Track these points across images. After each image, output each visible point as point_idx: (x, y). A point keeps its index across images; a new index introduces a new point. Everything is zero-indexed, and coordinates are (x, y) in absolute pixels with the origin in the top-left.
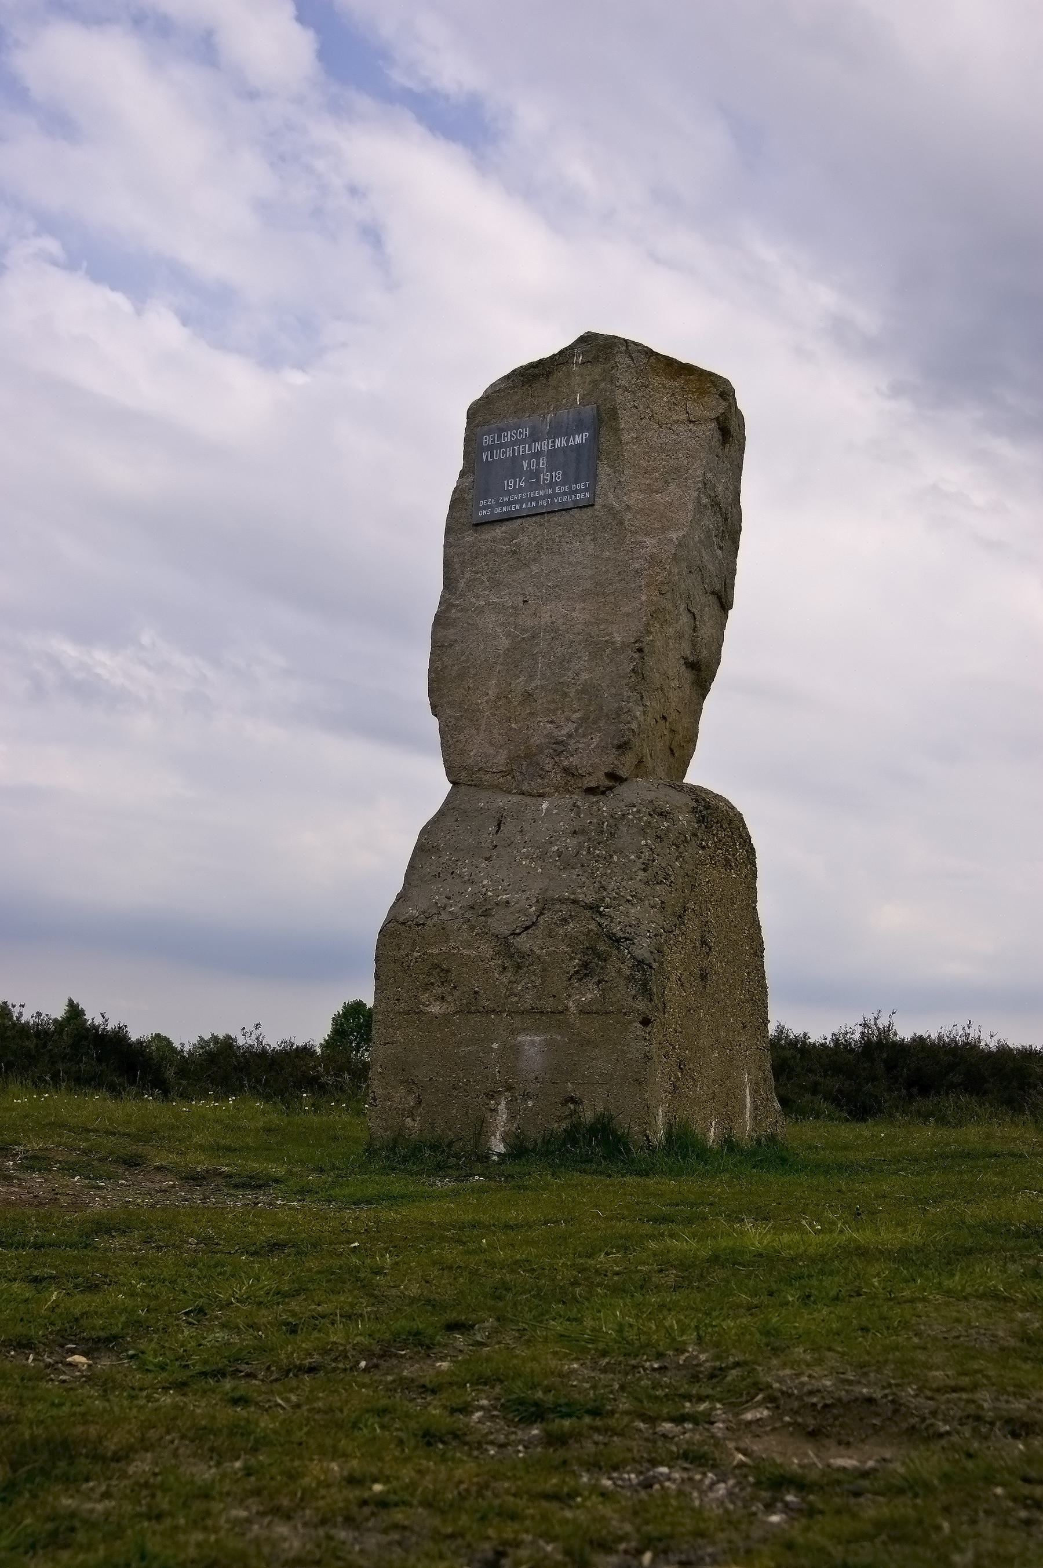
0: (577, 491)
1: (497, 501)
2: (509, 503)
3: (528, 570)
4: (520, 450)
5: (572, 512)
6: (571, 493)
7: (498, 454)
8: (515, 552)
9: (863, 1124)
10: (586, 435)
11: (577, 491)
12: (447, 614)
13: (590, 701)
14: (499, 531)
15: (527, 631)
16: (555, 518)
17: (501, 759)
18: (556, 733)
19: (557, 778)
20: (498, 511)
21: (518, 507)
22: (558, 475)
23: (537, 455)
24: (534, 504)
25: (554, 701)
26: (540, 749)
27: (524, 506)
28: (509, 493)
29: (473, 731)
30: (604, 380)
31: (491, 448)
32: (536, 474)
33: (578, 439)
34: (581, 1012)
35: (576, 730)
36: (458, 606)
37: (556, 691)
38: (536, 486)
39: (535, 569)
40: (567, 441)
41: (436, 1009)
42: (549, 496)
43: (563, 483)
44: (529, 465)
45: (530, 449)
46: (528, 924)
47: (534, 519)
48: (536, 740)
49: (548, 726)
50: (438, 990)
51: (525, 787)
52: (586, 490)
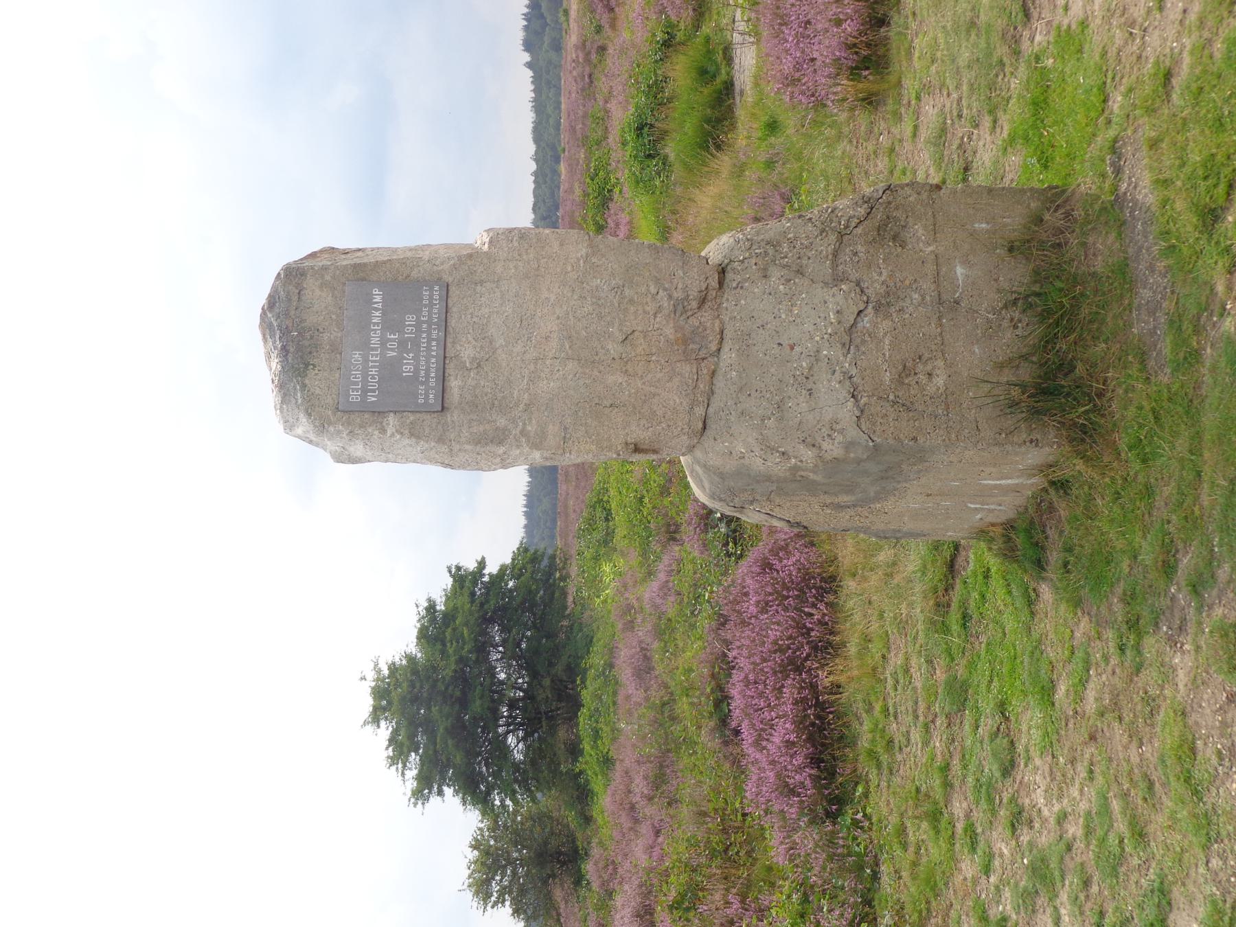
0: (431, 296)
1: (422, 383)
2: (428, 371)
3: (499, 351)
4: (374, 357)
5: (450, 305)
6: (431, 305)
7: (373, 384)
8: (479, 365)
9: (850, 584)
10: (376, 291)
11: (431, 296)
12: (532, 434)
13: (639, 275)
14: (454, 384)
15: (563, 345)
16: (453, 322)
17: (687, 369)
18: (666, 312)
19: (706, 316)
20: (432, 382)
21: (433, 360)
22: (410, 319)
23: (384, 342)
24: (434, 343)
25: (636, 312)
26: (678, 329)
27: (425, 326)
28: (417, 371)
29: (655, 401)
30: (322, 277)
31: (365, 391)
32: (402, 344)
33: (378, 299)
34: (935, 240)
35: (665, 290)
36: (524, 424)
37: (626, 310)
38: (416, 343)
39: (500, 342)
40: (377, 309)
41: (940, 381)
42: (430, 327)
43: (418, 312)
44: (392, 350)
45: (376, 349)
46: (858, 290)
47: (449, 345)
48: (669, 331)
49: (658, 319)
50: (923, 378)
51: (714, 347)
52: (431, 289)
